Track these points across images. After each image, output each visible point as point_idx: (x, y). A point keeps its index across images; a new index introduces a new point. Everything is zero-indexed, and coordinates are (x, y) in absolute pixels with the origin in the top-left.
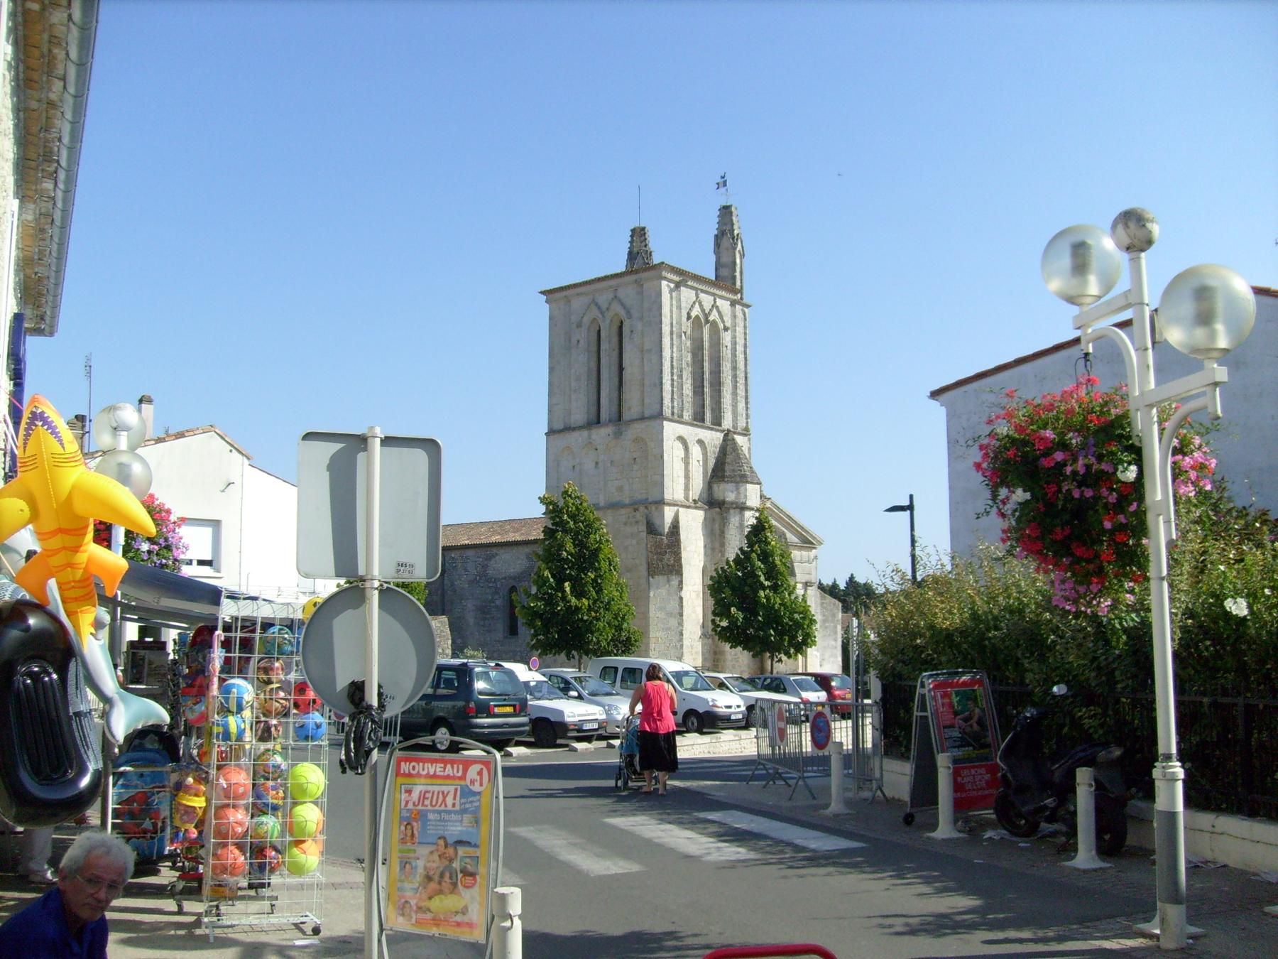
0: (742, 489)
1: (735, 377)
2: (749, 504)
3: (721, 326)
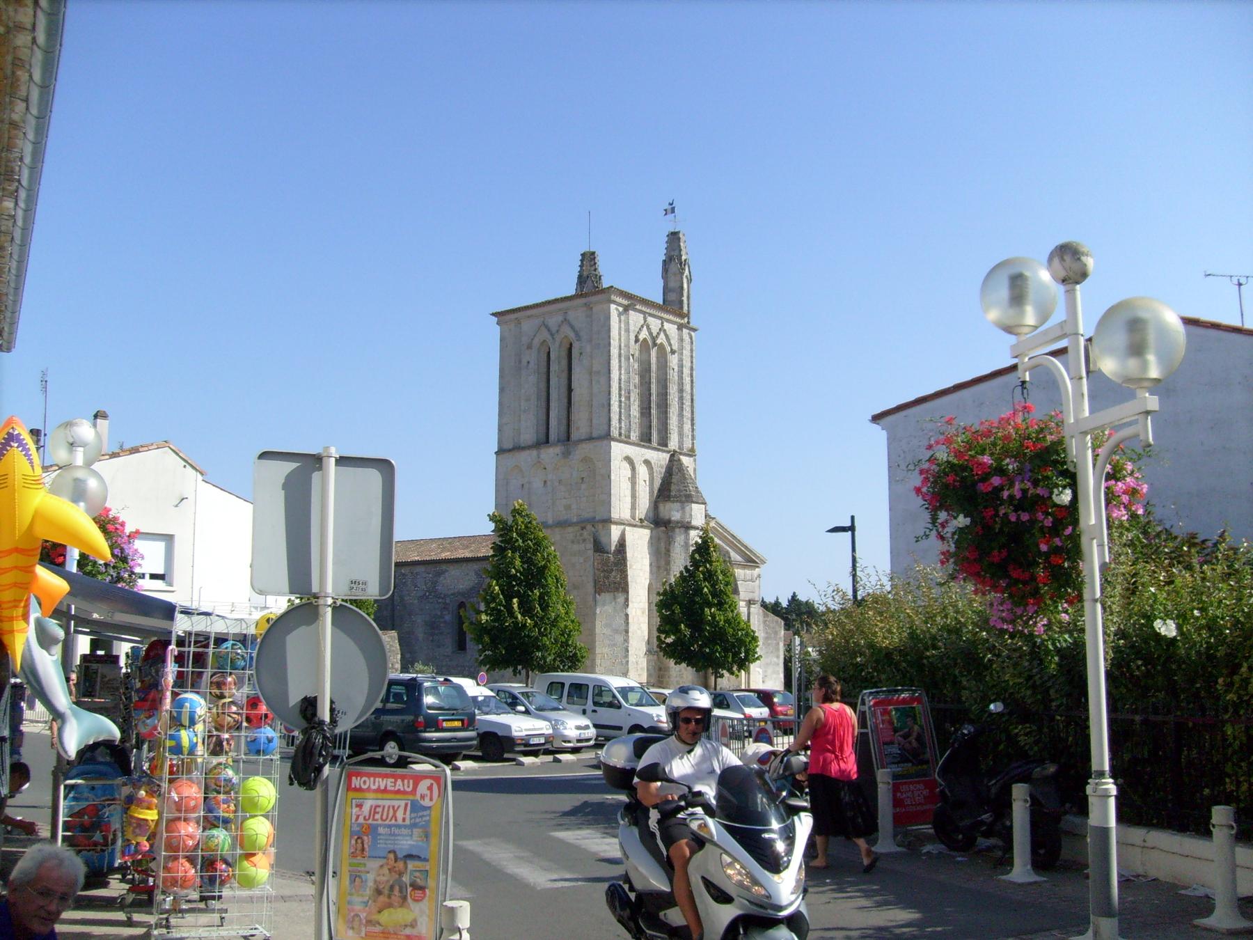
0: (687, 509)
1: (681, 399)
3: (668, 349)
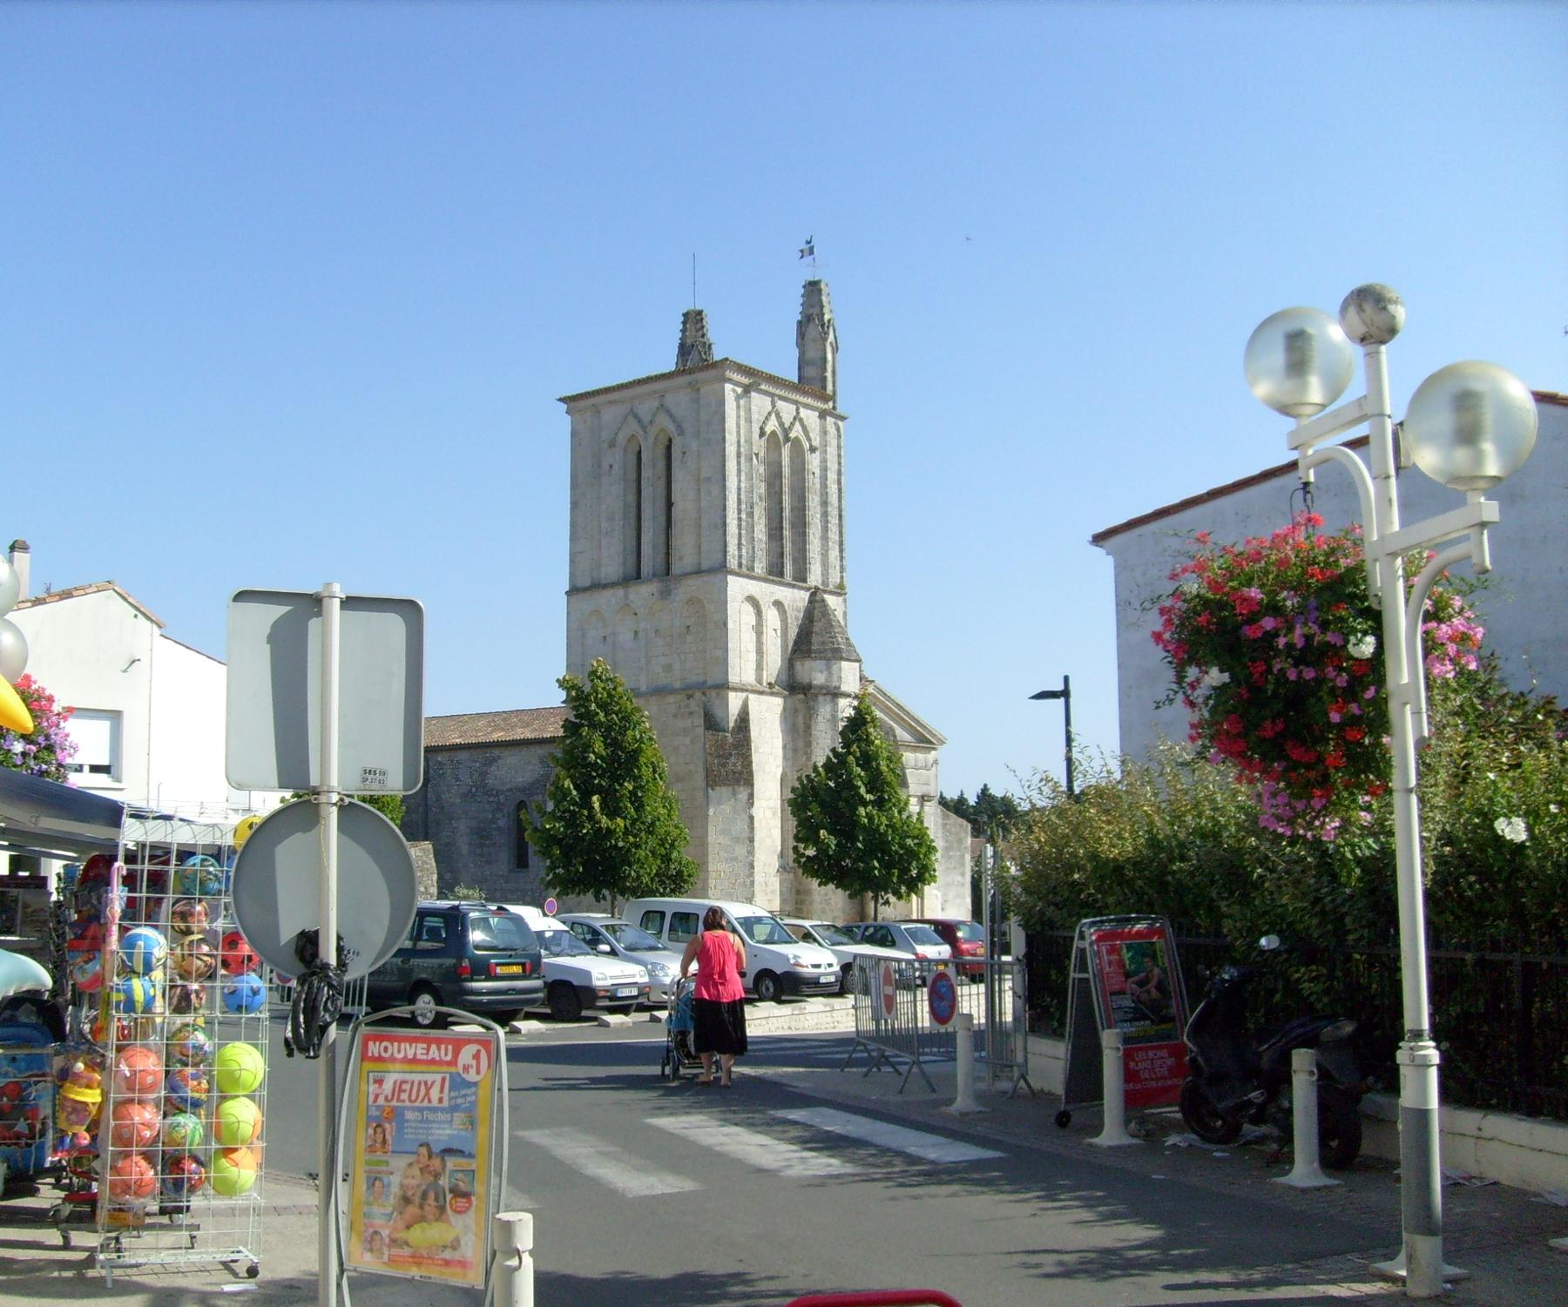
0: (835, 668)
1: (825, 514)
2: (844, 688)
3: (806, 445)
